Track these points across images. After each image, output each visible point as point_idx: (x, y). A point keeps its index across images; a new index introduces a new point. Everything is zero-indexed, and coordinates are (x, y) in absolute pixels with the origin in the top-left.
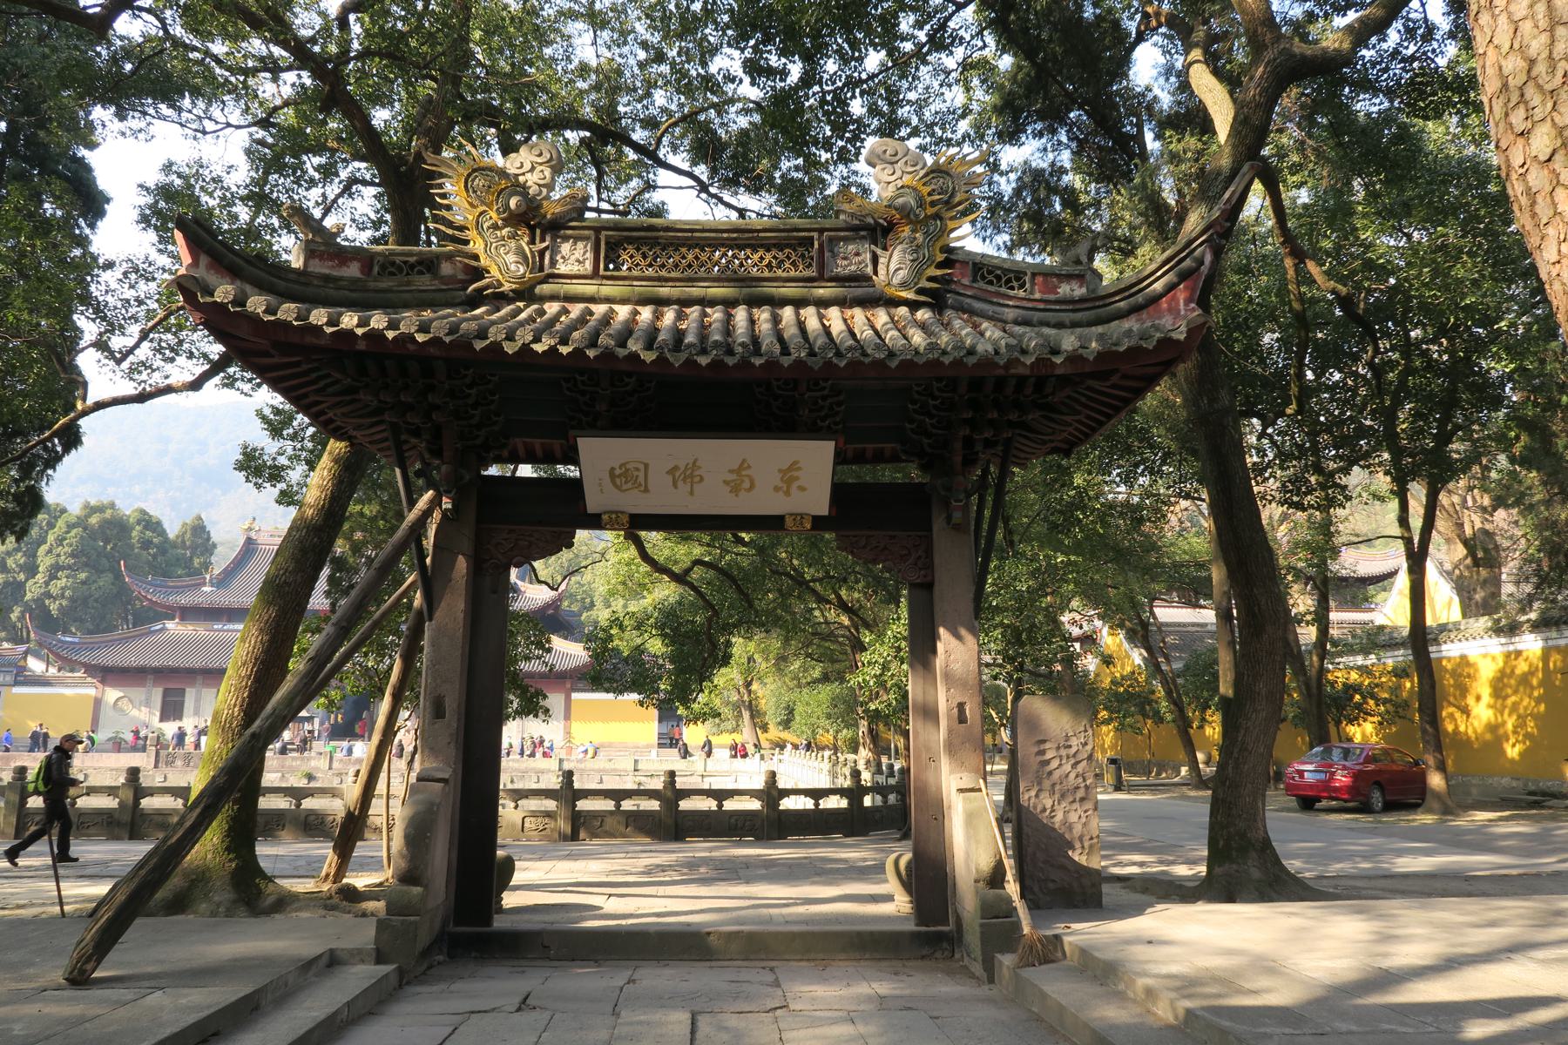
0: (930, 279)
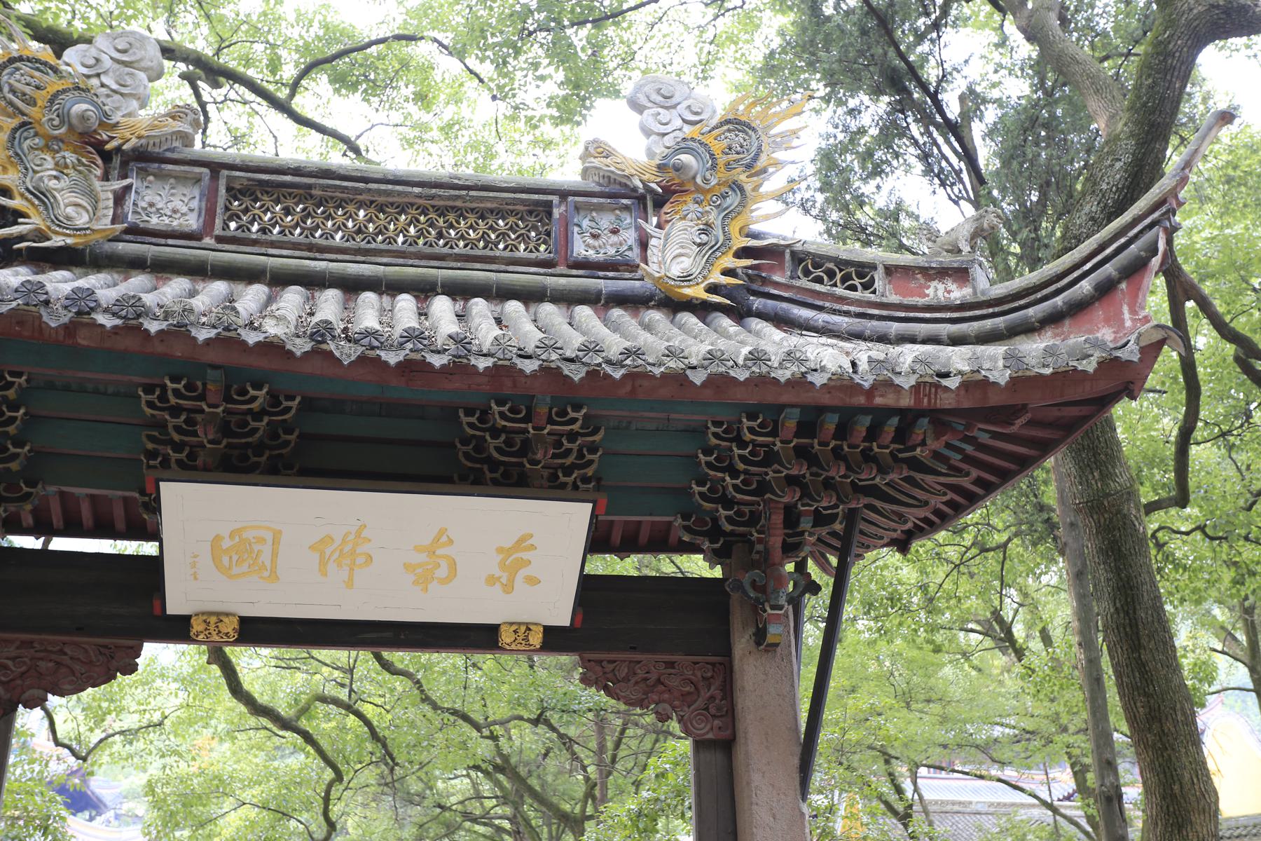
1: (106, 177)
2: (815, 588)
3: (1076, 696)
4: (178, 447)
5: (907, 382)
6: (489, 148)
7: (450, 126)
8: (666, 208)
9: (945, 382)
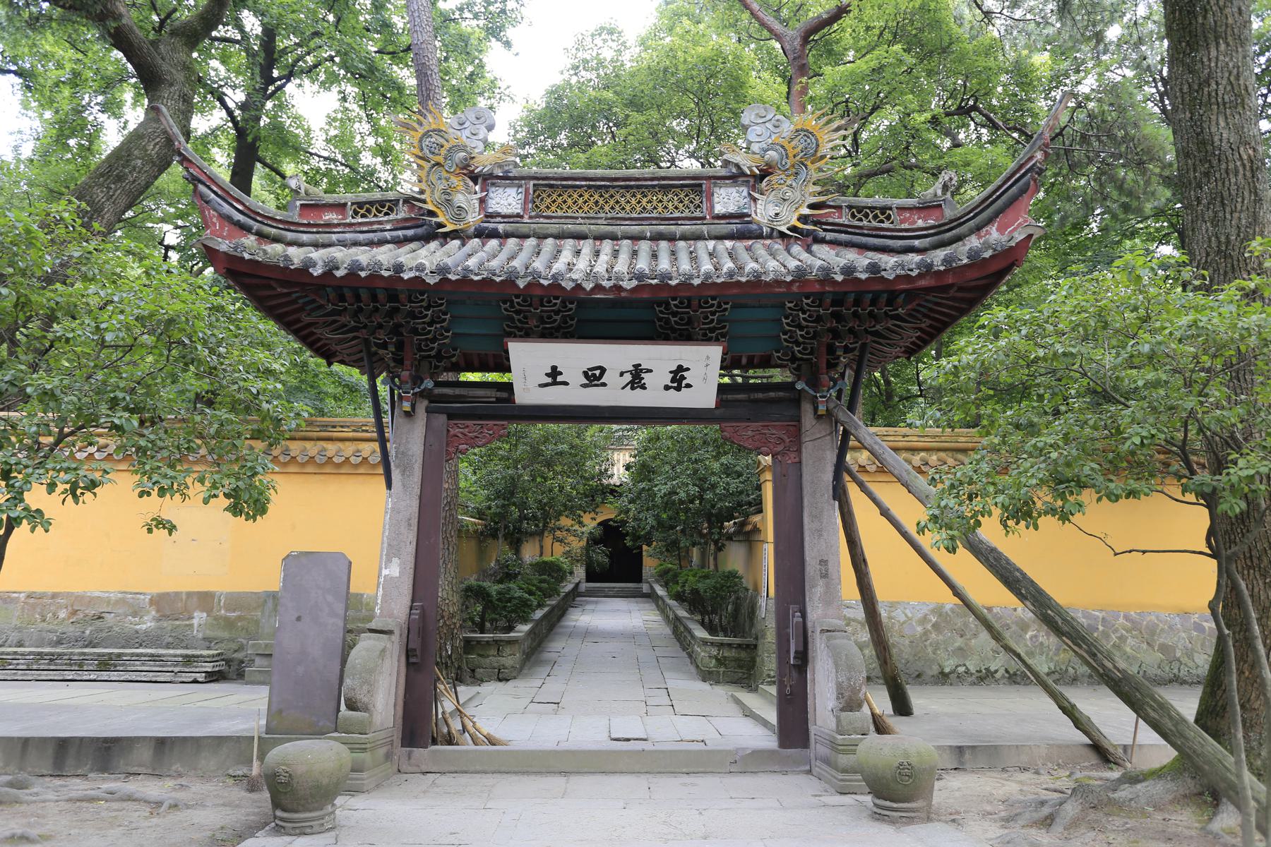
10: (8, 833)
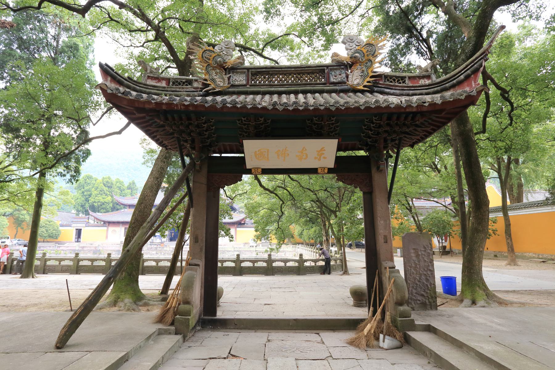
0: (368, 82)
1: (226, 74)
2: (391, 157)
3: (454, 181)
4: (246, 132)
5: (414, 105)
6: (308, 59)
7: (298, 55)
8: (353, 68)
9: (425, 104)
10: (510, 308)
